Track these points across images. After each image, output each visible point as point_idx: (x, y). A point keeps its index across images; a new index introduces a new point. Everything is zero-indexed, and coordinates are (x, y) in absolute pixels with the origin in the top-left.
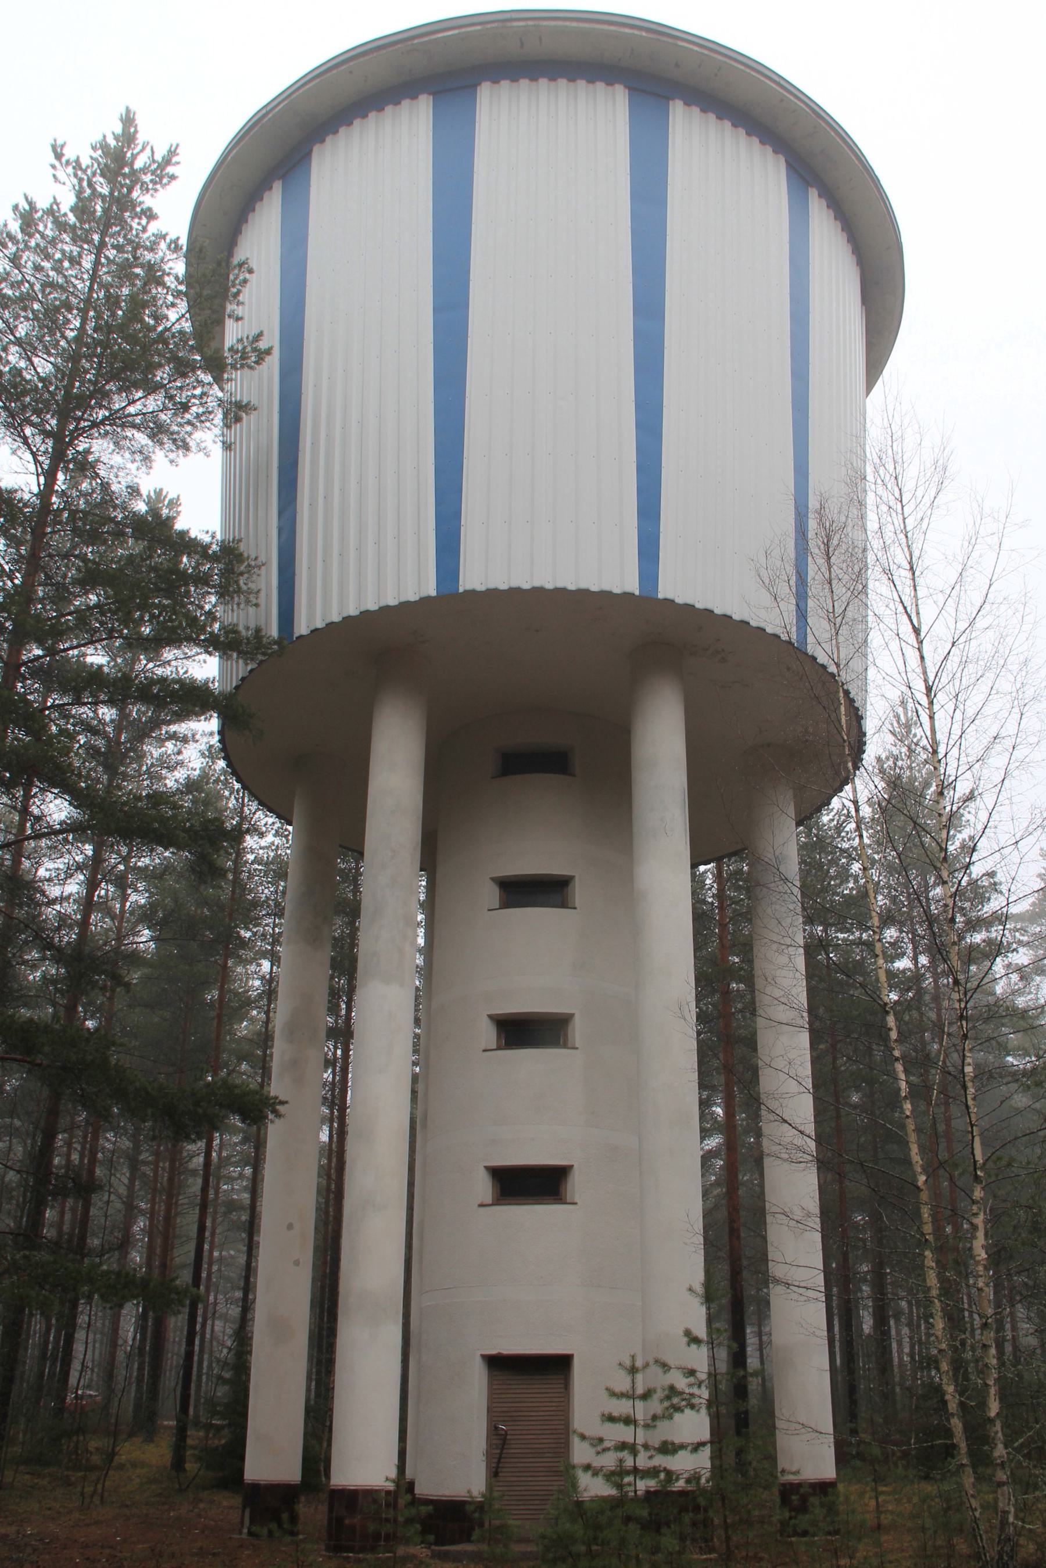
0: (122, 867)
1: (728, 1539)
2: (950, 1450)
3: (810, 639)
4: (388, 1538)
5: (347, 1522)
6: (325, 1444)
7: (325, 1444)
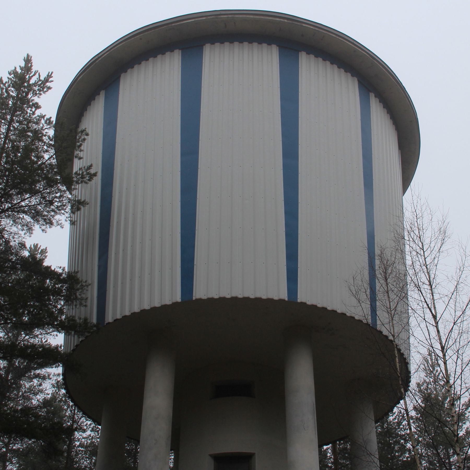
3: (378, 322)
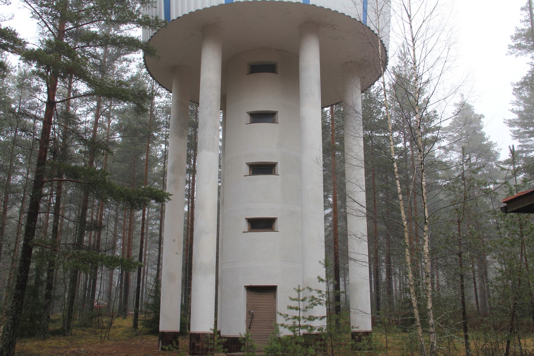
0: (108, 110)
1: (332, 350)
2: (413, 321)
3: (368, 20)
4: (211, 350)
5: (196, 344)
6: (188, 318)
7: (188, 318)
